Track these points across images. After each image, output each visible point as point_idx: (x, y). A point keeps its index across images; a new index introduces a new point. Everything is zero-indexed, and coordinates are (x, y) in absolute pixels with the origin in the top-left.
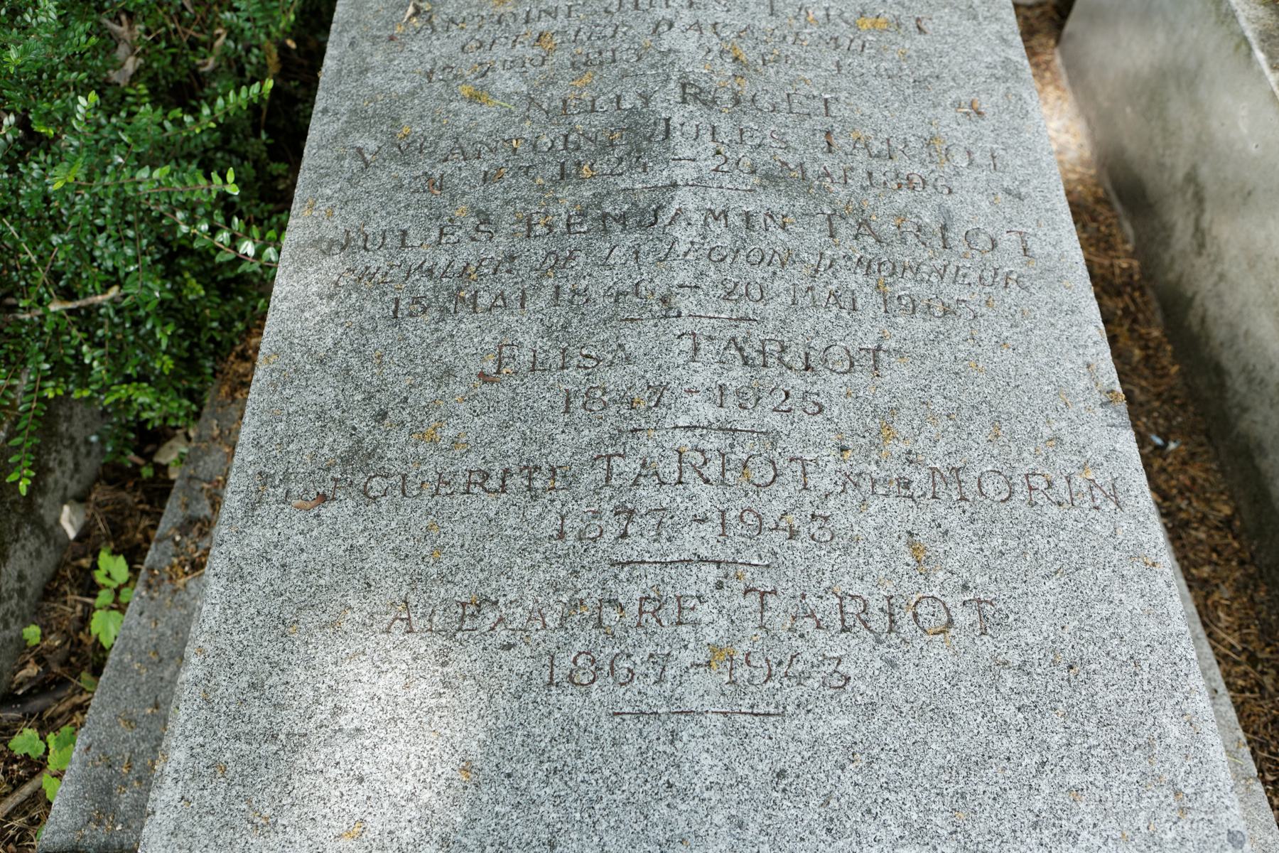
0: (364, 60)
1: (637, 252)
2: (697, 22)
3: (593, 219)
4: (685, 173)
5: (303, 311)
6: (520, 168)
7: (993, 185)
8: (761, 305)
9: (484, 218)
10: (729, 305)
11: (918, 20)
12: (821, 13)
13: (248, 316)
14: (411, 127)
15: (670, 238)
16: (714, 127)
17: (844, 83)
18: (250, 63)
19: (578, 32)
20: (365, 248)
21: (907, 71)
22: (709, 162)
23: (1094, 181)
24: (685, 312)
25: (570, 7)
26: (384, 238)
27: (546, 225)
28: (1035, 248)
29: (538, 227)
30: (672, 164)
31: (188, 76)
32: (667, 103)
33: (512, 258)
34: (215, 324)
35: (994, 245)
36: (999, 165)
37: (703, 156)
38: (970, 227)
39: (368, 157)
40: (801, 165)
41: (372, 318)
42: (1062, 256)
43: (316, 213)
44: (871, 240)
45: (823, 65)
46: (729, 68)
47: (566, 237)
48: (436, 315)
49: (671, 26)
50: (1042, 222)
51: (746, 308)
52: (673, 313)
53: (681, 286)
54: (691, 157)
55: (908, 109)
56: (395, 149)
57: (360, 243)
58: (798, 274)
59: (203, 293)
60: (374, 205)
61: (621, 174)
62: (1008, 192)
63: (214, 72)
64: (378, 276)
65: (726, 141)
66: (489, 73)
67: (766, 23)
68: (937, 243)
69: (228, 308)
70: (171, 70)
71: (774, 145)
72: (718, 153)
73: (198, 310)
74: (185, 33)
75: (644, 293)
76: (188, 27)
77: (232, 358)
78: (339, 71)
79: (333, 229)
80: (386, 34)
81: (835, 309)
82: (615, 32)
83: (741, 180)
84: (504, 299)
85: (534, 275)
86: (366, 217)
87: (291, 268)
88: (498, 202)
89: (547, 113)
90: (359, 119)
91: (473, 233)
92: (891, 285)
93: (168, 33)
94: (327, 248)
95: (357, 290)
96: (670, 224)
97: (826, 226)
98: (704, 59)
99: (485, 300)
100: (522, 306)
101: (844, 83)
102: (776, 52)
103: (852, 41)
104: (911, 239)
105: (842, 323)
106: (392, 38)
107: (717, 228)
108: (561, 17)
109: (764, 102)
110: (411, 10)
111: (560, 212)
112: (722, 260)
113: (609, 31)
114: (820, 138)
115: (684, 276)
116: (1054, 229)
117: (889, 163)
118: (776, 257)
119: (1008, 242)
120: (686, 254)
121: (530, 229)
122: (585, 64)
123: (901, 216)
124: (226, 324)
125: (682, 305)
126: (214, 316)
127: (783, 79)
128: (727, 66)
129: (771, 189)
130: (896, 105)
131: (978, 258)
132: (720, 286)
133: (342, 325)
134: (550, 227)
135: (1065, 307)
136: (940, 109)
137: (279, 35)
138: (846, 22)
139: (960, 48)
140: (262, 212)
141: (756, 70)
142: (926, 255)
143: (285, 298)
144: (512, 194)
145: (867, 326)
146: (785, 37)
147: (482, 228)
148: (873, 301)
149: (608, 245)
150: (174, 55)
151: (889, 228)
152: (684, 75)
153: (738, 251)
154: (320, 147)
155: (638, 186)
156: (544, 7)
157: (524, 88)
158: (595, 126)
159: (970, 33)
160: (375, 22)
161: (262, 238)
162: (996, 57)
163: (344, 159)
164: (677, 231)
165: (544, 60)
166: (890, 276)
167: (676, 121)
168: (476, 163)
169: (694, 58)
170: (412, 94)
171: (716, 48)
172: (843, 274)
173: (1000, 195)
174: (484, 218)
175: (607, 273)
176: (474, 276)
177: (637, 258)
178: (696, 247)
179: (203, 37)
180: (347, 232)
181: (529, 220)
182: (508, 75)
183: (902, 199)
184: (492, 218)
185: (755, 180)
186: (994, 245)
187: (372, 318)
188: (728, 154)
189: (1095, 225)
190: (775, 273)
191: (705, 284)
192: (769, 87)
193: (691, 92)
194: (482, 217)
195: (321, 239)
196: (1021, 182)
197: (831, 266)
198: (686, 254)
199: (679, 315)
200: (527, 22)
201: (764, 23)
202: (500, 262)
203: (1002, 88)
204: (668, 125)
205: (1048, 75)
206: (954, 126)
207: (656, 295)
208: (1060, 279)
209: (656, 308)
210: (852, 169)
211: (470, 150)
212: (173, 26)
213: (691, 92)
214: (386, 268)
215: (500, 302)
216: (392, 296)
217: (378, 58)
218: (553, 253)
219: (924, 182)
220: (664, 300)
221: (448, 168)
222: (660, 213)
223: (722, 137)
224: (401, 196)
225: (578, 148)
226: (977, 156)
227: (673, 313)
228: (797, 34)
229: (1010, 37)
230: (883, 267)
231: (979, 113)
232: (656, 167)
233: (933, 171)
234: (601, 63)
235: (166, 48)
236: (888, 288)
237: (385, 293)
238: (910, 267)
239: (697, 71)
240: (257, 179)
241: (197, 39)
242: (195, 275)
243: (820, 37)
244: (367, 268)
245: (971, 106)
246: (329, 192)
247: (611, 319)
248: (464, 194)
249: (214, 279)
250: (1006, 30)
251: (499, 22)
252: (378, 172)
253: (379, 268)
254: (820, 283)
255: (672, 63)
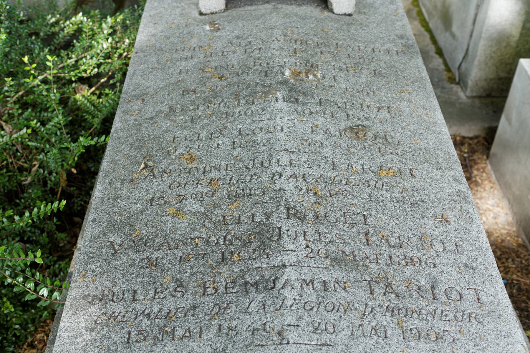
0: (116, 192)
1: (264, 305)
2: (294, 174)
3: (240, 285)
4: (290, 258)
5: (76, 338)
6: (200, 255)
7: (457, 262)
8: (333, 336)
9: (180, 283)
10: (316, 336)
11: (411, 170)
12: (359, 168)
13: (37, 321)
14: (141, 231)
15: (282, 297)
16: (305, 232)
17: (374, 206)
18: (51, 180)
19: (231, 178)
20: (113, 300)
21: (407, 198)
22: (303, 252)
23: (516, 234)
24: (291, 341)
25: (227, 165)
26: (123, 295)
27: (214, 288)
28: (484, 299)
29: (209, 289)
30: (283, 253)
31: (16, 186)
32: (279, 218)
33: (194, 308)
34: (17, 326)
35: (461, 297)
36: (460, 250)
37: (299, 249)
38: (447, 286)
39: (117, 247)
40: (353, 252)
41: (115, 343)
42: (499, 303)
43: (86, 280)
44: (393, 296)
45: (362, 196)
46: (312, 199)
47: (225, 295)
48: (151, 341)
49: (281, 176)
50: (486, 283)
51: (326, 338)
52: (285, 342)
53: (289, 325)
54: (293, 250)
55: (409, 219)
56: (132, 243)
57: (110, 297)
58: (353, 317)
59: (13, 310)
60: (119, 275)
61: (255, 259)
62: (466, 265)
63: (30, 184)
64: (120, 317)
65: (312, 240)
66: (184, 201)
67: (330, 174)
68: (430, 296)
69: (25, 317)
70: (7, 184)
71: (337, 241)
72: (308, 246)
73: (8, 319)
74: (16, 163)
75: (268, 329)
76: (19, 160)
77: (25, 347)
78: (103, 198)
79: (95, 289)
80: (129, 178)
81: (375, 337)
82: (251, 179)
83: (320, 262)
84: (190, 332)
85: (207, 318)
86: (114, 282)
87: (70, 312)
88: (187, 274)
89: (215, 223)
90: (113, 226)
91: (173, 292)
92: (406, 322)
93: (7, 164)
94: (91, 300)
95: (107, 325)
96: (282, 288)
97: (368, 288)
98: (299, 194)
99: (179, 333)
100: (200, 337)
101: (374, 206)
102: (336, 189)
103: (376, 182)
104: (415, 294)
105: (380, 346)
106: (132, 181)
107: (308, 290)
108: (222, 170)
109: (331, 217)
110: (143, 166)
111: (222, 280)
112: (311, 309)
113: (248, 179)
114: (362, 236)
115: (290, 319)
116: (493, 287)
117: (400, 251)
118: (341, 307)
119: (469, 295)
120: (291, 306)
121: (205, 291)
122: (235, 196)
123: (409, 281)
124: (24, 326)
125: (290, 337)
126: (17, 322)
127: (341, 204)
128: (311, 198)
129: (337, 267)
130: (402, 217)
131: (453, 305)
132: (311, 325)
133: (98, 347)
134: (216, 289)
135: (504, 333)
136: (426, 219)
137: (68, 167)
138: (373, 172)
139: (434, 185)
140: (51, 262)
141: (326, 200)
142: (424, 304)
143: (66, 330)
144: (195, 270)
145: (393, 347)
146: (341, 181)
147: (178, 289)
148: (396, 332)
149: (248, 300)
150: (9, 176)
151: (402, 288)
152: (288, 203)
153: (320, 304)
154: (90, 241)
155: (264, 266)
156: (213, 165)
157: (202, 209)
158: (241, 231)
159: (439, 177)
160: (123, 172)
161: (52, 284)
162: (453, 189)
163: (103, 248)
164: (286, 293)
165: (213, 194)
166: (405, 317)
167: (284, 229)
168: (176, 251)
169: (293, 194)
170: (142, 212)
171: (305, 188)
172: (379, 316)
173: (462, 268)
174: (180, 283)
175: (248, 317)
176: (173, 318)
177: (264, 308)
178: (297, 302)
179: (26, 165)
180: (103, 291)
181: (205, 285)
182: (193, 202)
183: (409, 270)
184: (184, 283)
185: (328, 262)
186: (461, 297)
187: (115, 343)
188: (313, 247)
189: (519, 260)
190: (341, 317)
191: (302, 323)
192: (334, 209)
193: (293, 213)
194: (179, 283)
195: (88, 295)
196: (473, 260)
197: (372, 311)
198: (291, 306)
199: (288, 343)
200: (204, 173)
201: (330, 174)
202: (188, 310)
203: (458, 207)
204: (280, 231)
205: (484, 175)
206: (434, 228)
207: (275, 331)
208: (499, 316)
209: (275, 338)
210: (380, 254)
211: (172, 244)
212: (10, 160)
213: (293, 213)
214: (124, 313)
215: (187, 334)
216: (126, 329)
217: (124, 191)
218: (218, 305)
219: (420, 261)
220: (280, 333)
221: (160, 254)
222: (277, 282)
223: (309, 238)
224: (134, 270)
225: (231, 244)
226: (447, 245)
227: (285, 342)
228: (347, 179)
229: (460, 178)
230: (401, 312)
231: (447, 221)
232: (274, 255)
233: (424, 255)
234: (244, 196)
235: (6, 173)
236: (404, 324)
237: (123, 328)
238: (416, 311)
239: (295, 201)
240: (49, 243)
241: (23, 166)
242: (8, 299)
243: (360, 180)
244: (113, 313)
245: (442, 217)
246: (94, 267)
247: (250, 345)
248: (169, 269)
249: (19, 301)
250: (458, 175)
251: (189, 172)
252: (122, 256)
253: (120, 313)
254: (366, 322)
255: (282, 197)
